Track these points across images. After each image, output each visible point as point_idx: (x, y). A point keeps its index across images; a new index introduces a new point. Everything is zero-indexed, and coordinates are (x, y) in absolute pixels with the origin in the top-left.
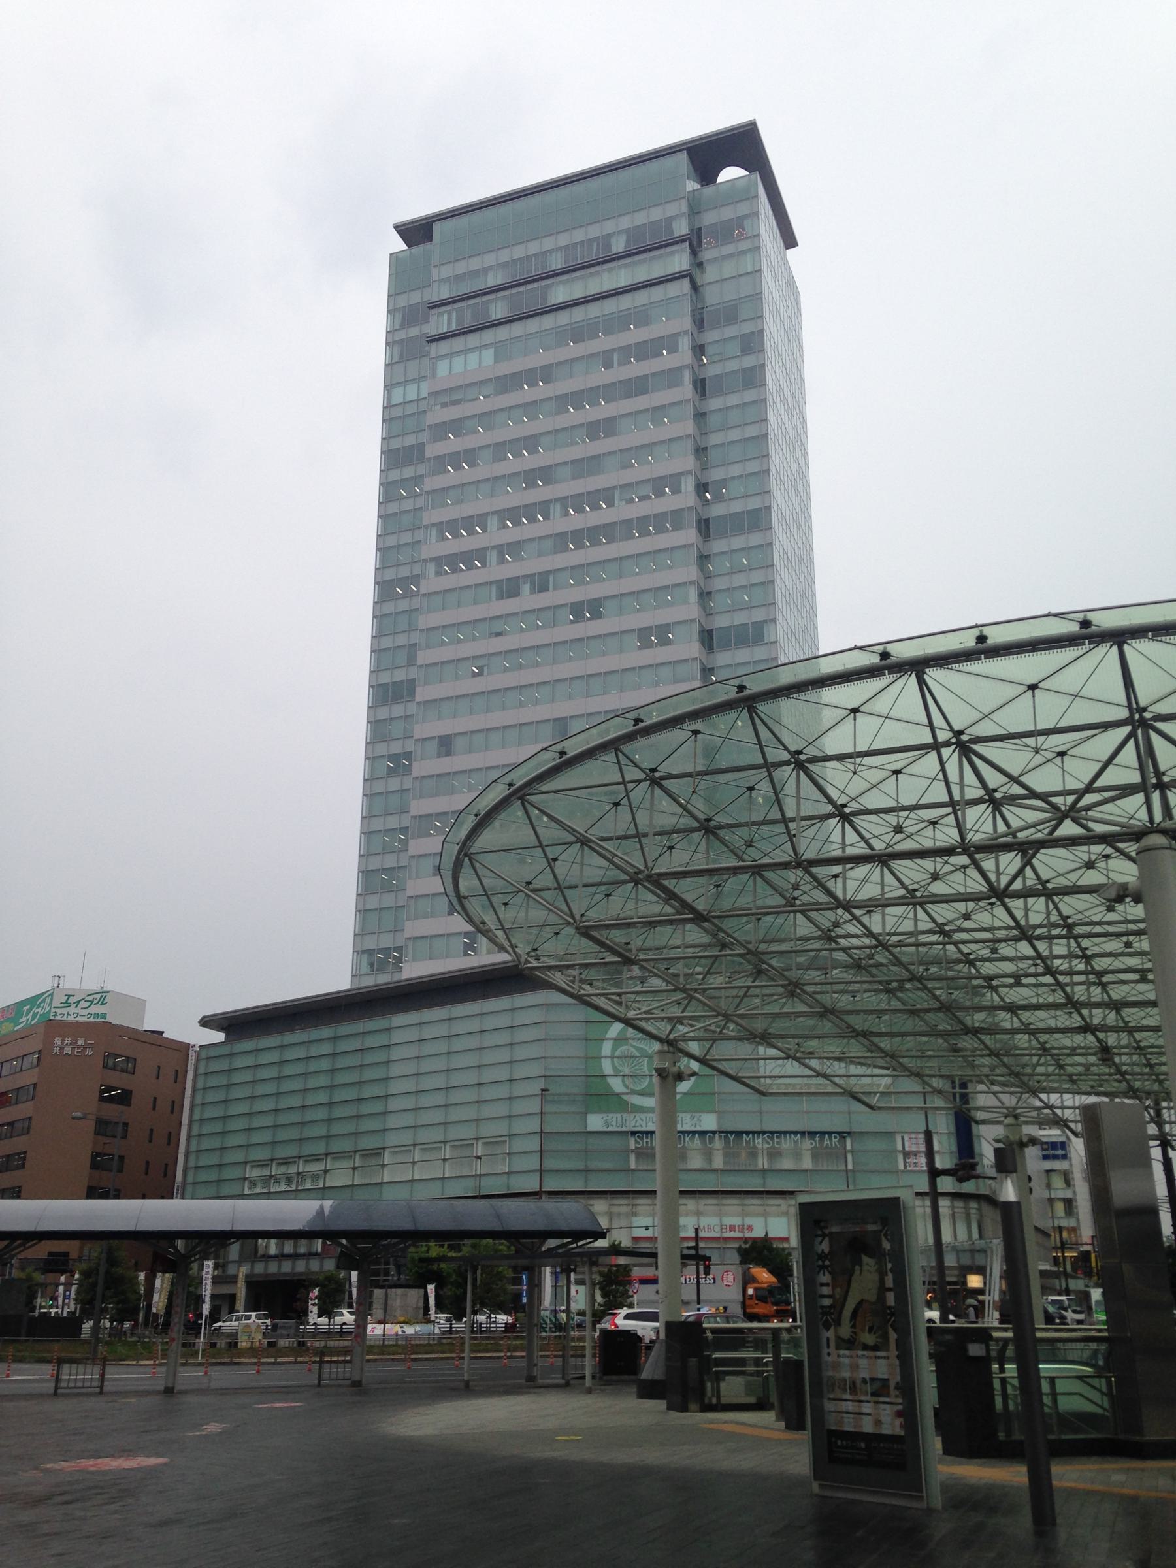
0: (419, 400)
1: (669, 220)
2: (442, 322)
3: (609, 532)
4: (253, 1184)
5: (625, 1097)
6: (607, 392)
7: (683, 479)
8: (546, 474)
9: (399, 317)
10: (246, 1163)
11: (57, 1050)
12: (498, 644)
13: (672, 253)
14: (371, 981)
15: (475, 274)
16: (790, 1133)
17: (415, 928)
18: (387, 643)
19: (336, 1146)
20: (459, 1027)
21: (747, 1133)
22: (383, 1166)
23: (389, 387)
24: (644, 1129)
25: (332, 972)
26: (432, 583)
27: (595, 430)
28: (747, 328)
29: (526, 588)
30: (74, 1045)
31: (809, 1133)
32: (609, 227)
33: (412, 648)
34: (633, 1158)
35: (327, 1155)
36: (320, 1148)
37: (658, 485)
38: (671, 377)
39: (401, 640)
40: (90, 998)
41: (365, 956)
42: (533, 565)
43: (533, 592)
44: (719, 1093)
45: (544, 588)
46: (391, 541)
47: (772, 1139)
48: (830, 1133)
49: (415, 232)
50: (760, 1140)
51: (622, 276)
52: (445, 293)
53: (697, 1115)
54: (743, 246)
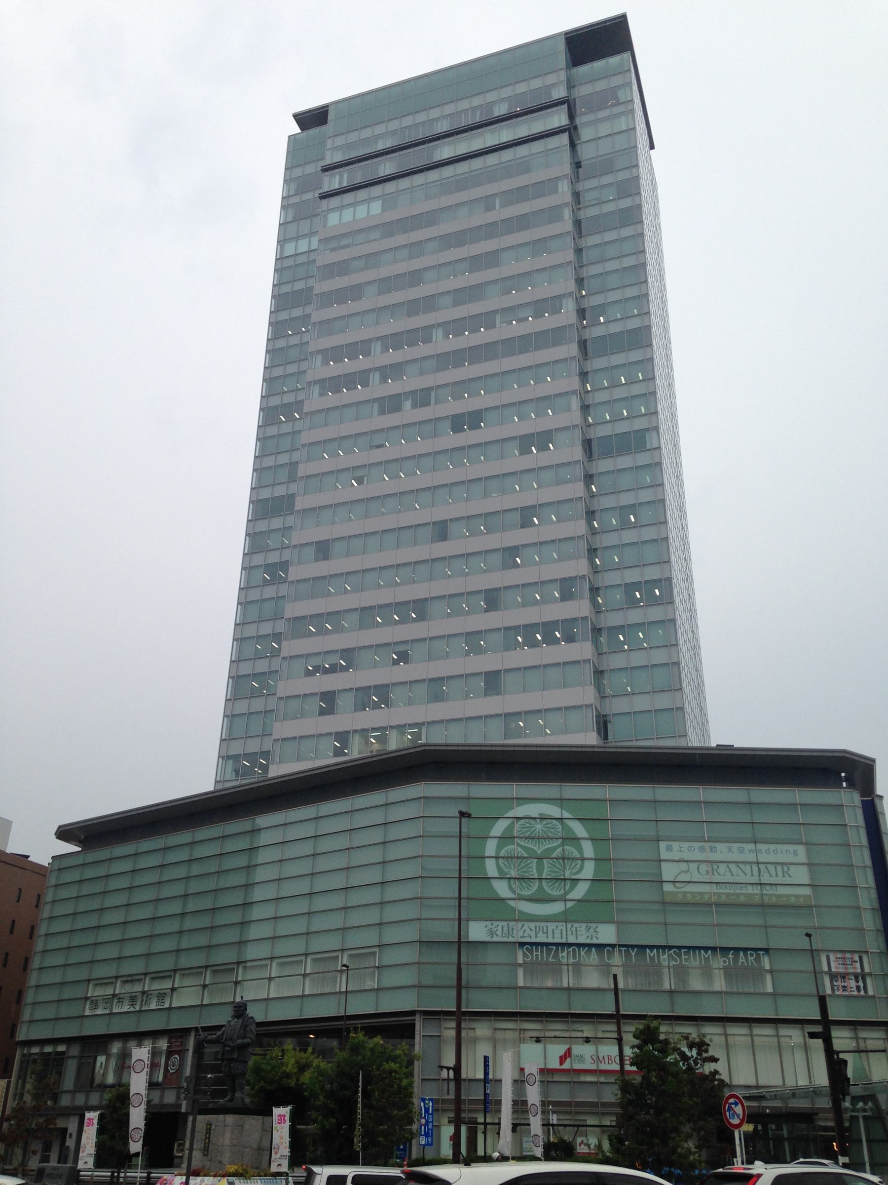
0: (310, 251)
2: (334, 181)
3: (489, 351)
4: (95, 1004)
6: (490, 230)
7: (564, 302)
8: (428, 303)
9: (293, 186)
10: (89, 981)
12: (377, 455)
14: (233, 783)
15: (366, 141)
16: (699, 948)
17: (283, 729)
18: (269, 462)
19: (185, 961)
21: (652, 947)
23: (282, 242)
24: (534, 940)
25: (196, 773)
26: (315, 401)
27: (476, 263)
28: (622, 176)
29: (408, 405)
31: (722, 949)
33: (294, 465)
34: (520, 972)
35: (175, 971)
36: (167, 963)
37: (540, 307)
38: (553, 214)
39: (284, 459)
41: (230, 763)
42: (412, 382)
43: (414, 406)
44: (617, 902)
45: (426, 403)
46: (278, 372)
48: (745, 950)
49: (312, 119)
50: (666, 956)
51: (505, 134)
52: (338, 158)
53: (594, 925)
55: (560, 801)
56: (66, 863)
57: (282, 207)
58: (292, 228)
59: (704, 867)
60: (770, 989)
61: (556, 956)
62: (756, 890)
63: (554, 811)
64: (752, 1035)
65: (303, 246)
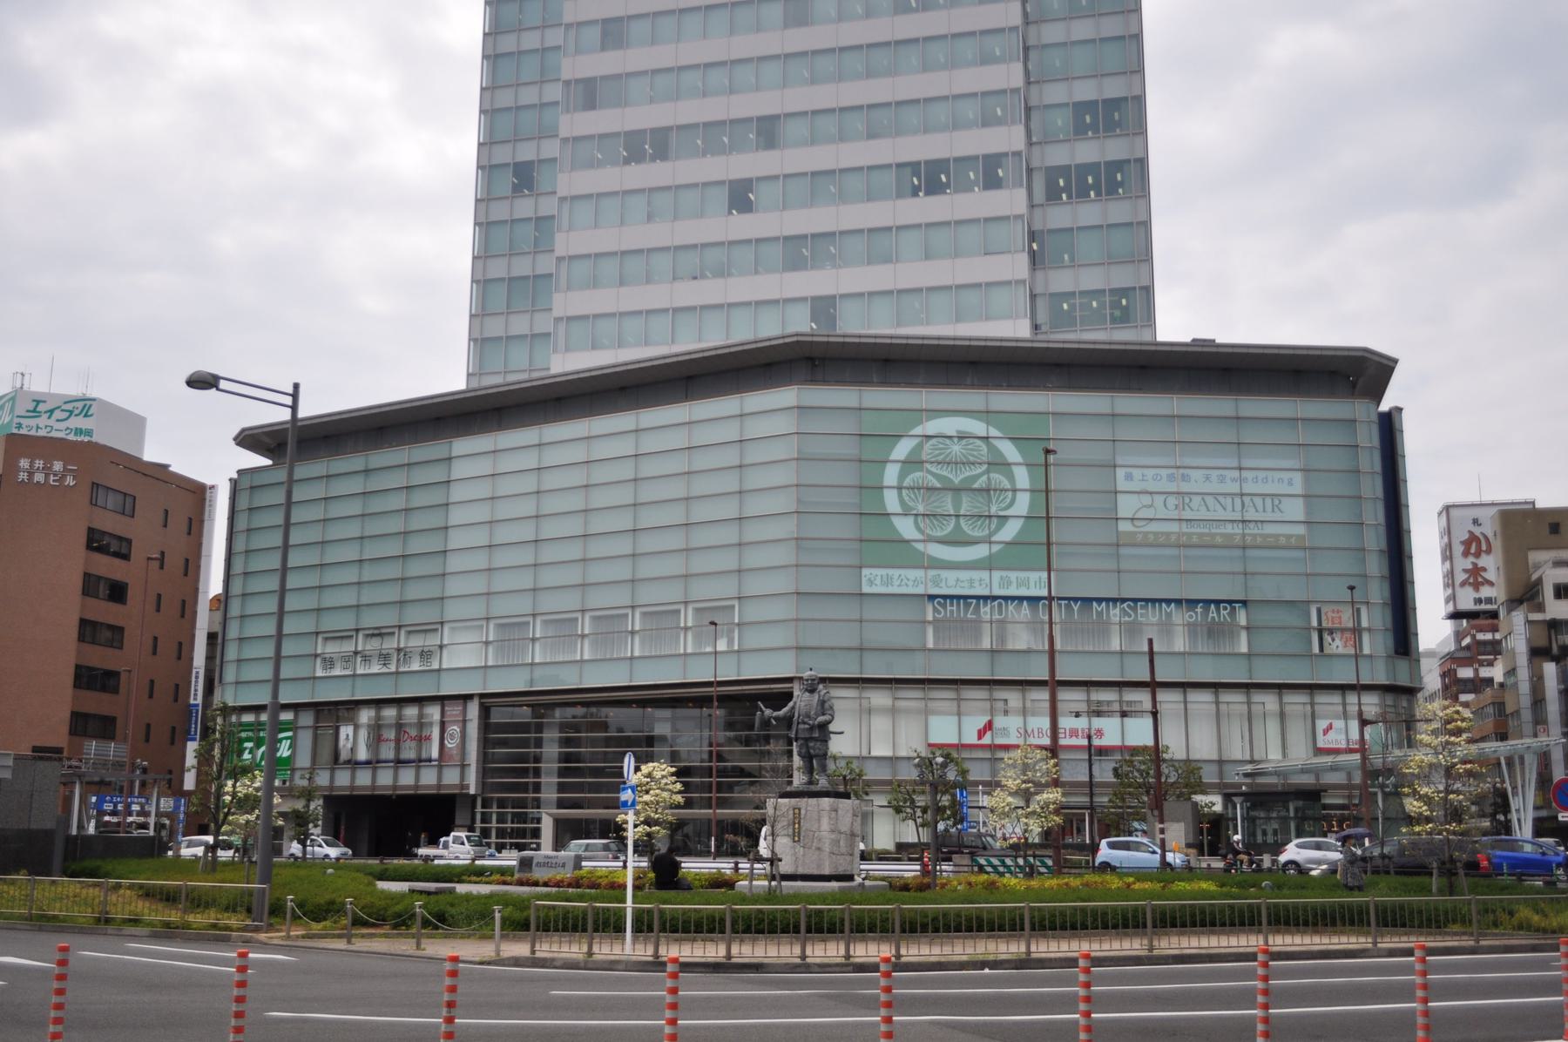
4: (329, 662)
5: (920, 546)
11: (23, 476)
16: (1160, 601)
21: (1099, 600)
22: (534, 640)
30: (47, 470)
31: (1188, 601)
34: (930, 631)
36: (345, 622)
40: (69, 407)
47: (1134, 609)
48: (1217, 602)
50: (1117, 611)
55: (986, 415)
59: (1172, 501)
60: (1244, 649)
62: (1237, 529)
63: (977, 427)
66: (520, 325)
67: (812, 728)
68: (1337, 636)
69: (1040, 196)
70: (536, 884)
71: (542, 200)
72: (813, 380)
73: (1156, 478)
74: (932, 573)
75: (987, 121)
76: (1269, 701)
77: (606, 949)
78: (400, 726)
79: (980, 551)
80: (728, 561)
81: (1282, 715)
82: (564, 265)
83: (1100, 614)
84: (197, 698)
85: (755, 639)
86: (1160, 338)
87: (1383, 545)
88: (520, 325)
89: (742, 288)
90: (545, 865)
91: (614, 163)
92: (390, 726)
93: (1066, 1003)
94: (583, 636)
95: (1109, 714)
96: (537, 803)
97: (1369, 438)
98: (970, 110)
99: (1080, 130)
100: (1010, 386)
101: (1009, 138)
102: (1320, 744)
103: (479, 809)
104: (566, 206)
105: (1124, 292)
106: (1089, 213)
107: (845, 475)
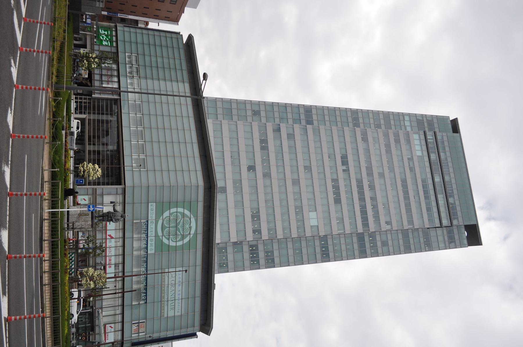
1: (457, 219)
2: (430, 136)
4: (130, 57)
5: (161, 218)
9: (430, 119)
13: (448, 220)
15: (444, 148)
16: (147, 281)
20: (185, 120)
21: (147, 265)
22: (136, 114)
29: (344, 168)
32: (456, 197)
36: (141, 62)
48: (146, 296)
49: (455, 126)
52: (439, 138)
54: (447, 243)
55: (196, 233)
56: (180, 40)
57: (422, 115)
58: (415, 119)
59: (173, 282)
60: (133, 303)
61: (144, 233)
62: (166, 299)
63: (193, 232)
64: (118, 306)
65: (407, 123)
66: (220, 111)
67: (111, 217)
68: (137, 327)
69: (251, 243)
70: (66, 138)
71: (251, 117)
72: (205, 189)
73: (179, 278)
74: (154, 221)
75: (269, 230)
76: (119, 311)
77: (46, 204)
78: (112, 76)
79: (160, 234)
80: (157, 167)
81: (115, 315)
82: (235, 123)
83: (143, 265)
84: (120, 15)
85: (136, 175)
86: (215, 275)
87: (161, 337)
88: (220, 111)
89: (229, 168)
90: (71, 139)
91: (260, 136)
92: (112, 73)
93: (29, 250)
94: (137, 128)
95: (115, 269)
96: (89, 113)
97: (190, 331)
98: (269, 197)
99: (266, 252)
100: (203, 239)
101: (265, 235)
102: (107, 325)
103: (88, 97)
104: (250, 124)
105: (227, 266)
106: (247, 256)
107: (180, 198)
